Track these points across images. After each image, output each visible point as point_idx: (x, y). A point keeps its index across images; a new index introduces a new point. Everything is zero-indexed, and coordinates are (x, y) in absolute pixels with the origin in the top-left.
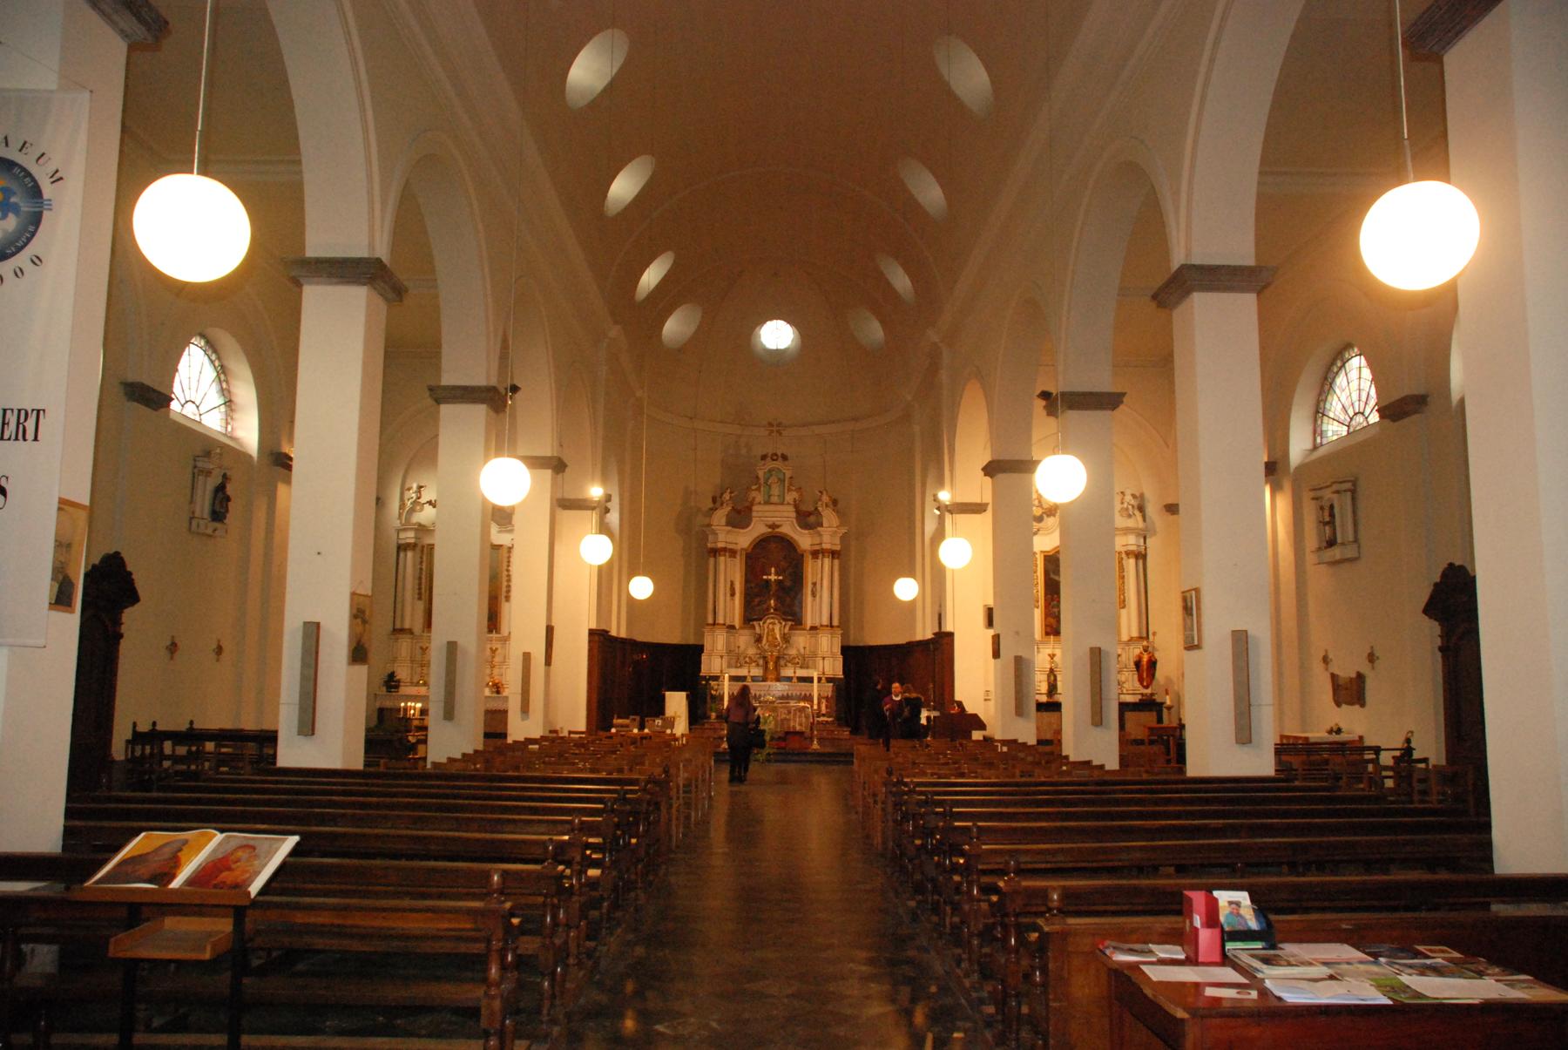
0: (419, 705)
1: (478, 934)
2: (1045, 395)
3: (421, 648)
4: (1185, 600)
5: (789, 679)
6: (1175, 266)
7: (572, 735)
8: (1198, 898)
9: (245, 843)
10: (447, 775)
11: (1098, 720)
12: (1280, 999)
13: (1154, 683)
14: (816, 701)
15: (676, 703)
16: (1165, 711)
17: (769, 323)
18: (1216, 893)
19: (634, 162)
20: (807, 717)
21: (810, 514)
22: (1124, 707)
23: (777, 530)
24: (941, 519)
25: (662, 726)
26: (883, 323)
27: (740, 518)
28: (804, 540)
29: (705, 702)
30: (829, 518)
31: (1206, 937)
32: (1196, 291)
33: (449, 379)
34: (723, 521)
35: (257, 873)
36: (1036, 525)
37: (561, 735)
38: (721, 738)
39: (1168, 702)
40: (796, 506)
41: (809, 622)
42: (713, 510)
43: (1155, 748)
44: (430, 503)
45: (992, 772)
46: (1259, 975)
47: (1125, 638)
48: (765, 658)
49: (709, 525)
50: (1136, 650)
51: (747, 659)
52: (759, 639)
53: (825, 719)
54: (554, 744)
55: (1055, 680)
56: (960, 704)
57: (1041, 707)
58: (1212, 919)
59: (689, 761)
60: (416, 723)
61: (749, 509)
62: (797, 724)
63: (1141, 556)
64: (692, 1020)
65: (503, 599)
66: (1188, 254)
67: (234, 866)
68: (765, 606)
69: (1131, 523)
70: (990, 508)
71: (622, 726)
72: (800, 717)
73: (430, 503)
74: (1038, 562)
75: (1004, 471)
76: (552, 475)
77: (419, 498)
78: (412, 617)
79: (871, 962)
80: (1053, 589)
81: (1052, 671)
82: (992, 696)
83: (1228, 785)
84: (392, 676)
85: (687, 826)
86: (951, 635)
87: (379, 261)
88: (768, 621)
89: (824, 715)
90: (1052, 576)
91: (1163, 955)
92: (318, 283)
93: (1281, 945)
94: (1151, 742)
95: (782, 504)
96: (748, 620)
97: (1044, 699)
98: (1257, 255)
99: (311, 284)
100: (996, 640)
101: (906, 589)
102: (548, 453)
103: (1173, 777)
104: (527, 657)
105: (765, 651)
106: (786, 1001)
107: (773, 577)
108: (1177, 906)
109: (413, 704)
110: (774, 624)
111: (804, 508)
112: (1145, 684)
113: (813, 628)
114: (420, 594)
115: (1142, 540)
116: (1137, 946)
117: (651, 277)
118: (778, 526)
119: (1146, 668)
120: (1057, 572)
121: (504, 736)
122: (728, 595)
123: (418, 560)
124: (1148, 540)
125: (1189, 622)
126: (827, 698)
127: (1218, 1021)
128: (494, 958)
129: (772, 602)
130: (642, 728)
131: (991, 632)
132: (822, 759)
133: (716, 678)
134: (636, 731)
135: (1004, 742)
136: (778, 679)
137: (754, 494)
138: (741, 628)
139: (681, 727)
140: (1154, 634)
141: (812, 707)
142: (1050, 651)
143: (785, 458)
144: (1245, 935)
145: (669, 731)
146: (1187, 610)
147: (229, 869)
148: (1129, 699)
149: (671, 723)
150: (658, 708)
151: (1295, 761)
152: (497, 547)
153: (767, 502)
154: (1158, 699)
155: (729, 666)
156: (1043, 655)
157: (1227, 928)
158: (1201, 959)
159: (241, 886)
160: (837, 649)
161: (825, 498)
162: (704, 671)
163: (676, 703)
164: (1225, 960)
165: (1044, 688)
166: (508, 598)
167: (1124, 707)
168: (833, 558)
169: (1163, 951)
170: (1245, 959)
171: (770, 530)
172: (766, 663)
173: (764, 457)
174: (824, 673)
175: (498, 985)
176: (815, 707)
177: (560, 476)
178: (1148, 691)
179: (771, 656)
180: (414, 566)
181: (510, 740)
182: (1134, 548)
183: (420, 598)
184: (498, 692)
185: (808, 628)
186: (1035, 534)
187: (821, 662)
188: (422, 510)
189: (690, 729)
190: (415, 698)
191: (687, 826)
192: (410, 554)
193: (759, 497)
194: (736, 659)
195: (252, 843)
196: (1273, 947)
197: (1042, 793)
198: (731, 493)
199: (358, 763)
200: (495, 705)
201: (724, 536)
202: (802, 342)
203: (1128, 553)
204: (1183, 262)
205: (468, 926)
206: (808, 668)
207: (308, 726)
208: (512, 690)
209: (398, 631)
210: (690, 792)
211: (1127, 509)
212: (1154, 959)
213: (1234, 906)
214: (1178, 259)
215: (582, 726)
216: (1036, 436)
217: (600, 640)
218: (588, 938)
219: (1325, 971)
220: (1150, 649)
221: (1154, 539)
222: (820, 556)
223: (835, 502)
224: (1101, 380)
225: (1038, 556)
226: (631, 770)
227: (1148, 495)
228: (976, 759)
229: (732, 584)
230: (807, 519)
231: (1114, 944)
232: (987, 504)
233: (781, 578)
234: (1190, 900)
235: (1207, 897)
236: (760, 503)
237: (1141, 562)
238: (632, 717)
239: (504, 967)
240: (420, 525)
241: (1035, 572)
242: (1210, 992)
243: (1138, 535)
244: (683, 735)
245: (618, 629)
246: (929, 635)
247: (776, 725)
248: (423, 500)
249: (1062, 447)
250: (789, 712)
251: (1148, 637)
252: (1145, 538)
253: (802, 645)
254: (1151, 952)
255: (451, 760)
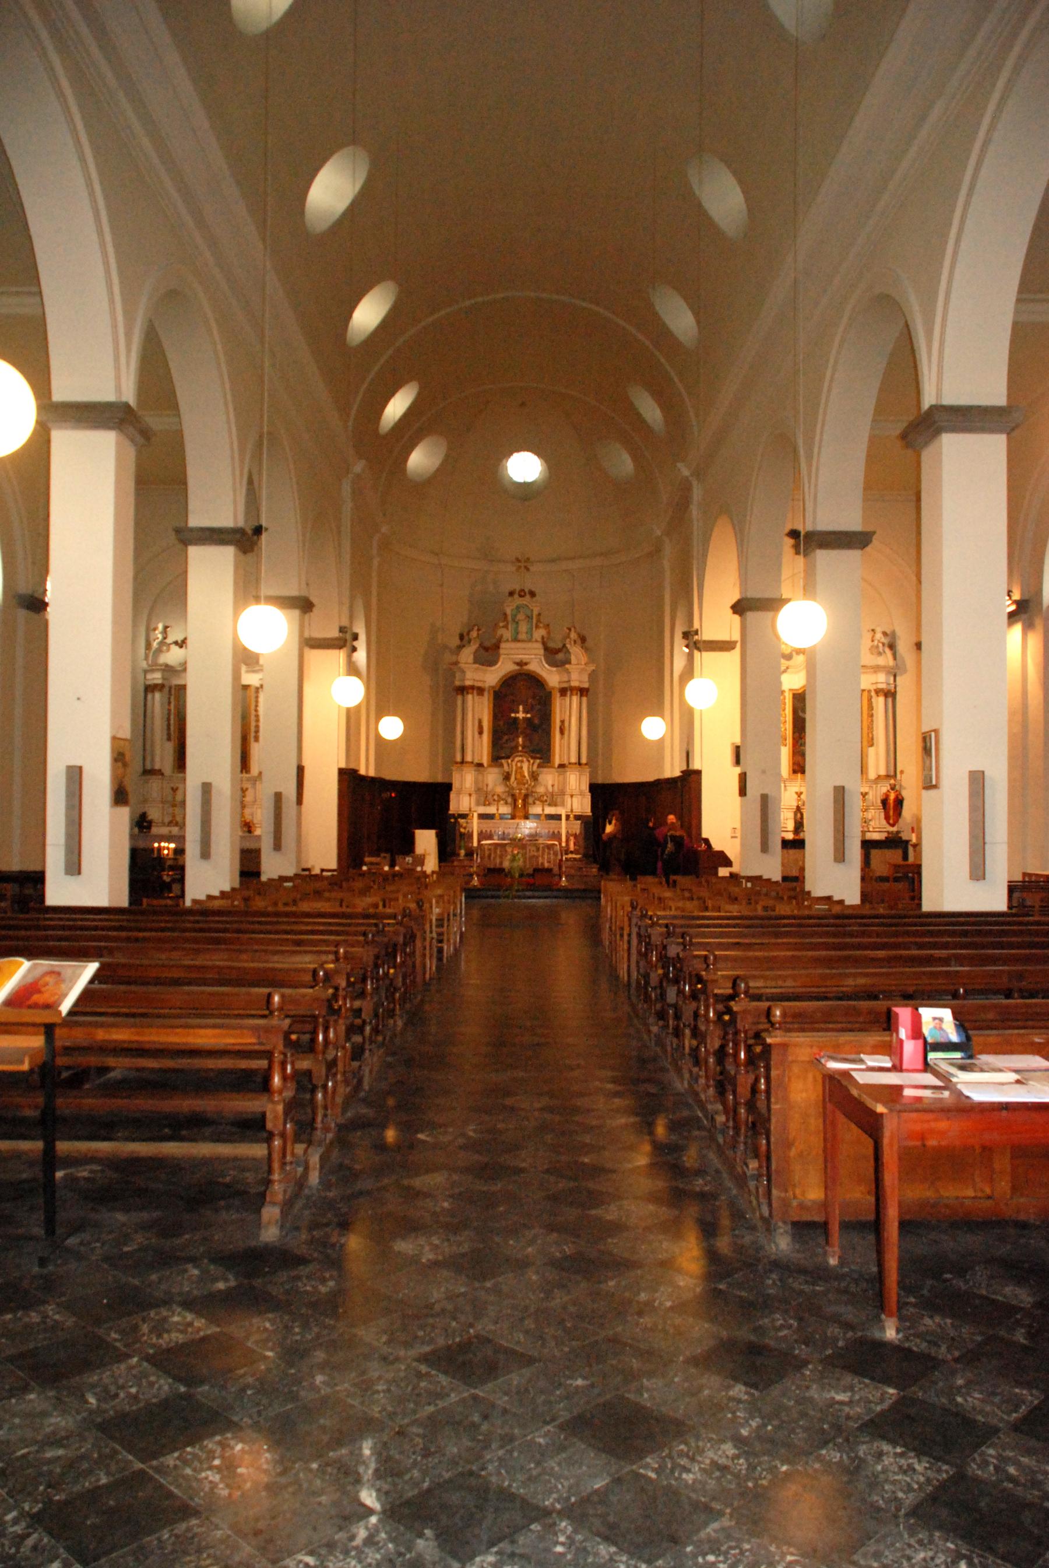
0: (172, 846)
1: (262, 1048)
2: (794, 534)
3: (172, 789)
4: (924, 739)
5: (538, 816)
6: (926, 404)
7: (325, 874)
8: (904, 1014)
9: (50, 969)
10: (203, 911)
11: (840, 856)
12: (968, 1097)
13: (900, 820)
14: (564, 839)
15: (426, 841)
16: (911, 849)
17: (515, 455)
18: (921, 1010)
19: (335, 157)
20: (555, 854)
21: (558, 651)
22: (868, 845)
23: (525, 667)
24: (690, 657)
25: (412, 864)
26: (635, 458)
27: (488, 654)
28: (553, 678)
29: (454, 840)
30: (577, 654)
31: (910, 1048)
32: (946, 432)
33: (196, 520)
34: (471, 659)
35: (65, 995)
36: (784, 663)
37: (313, 873)
38: (471, 875)
39: (914, 840)
40: (544, 643)
41: (557, 762)
42: (460, 647)
43: (900, 886)
44: (176, 643)
45: (736, 906)
46: (954, 1080)
47: (872, 775)
48: (513, 796)
49: (456, 663)
50: (883, 788)
51: (496, 797)
52: (507, 777)
53: (574, 856)
54: (306, 878)
55: (802, 818)
56: (707, 841)
57: (786, 844)
58: (917, 1033)
59: (441, 896)
60: (169, 863)
61: (497, 647)
62: (546, 861)
63: (890, 694)
64: (451, 1130)
65: (252, 740)
66: (939, 394)
67: (43, 989)
68: (513, 744)
69: (881, 661)
70: (738, 645)
71: (372, 864)
72: (549, 854)
73: (176, 643)
74: (787, 701)
75: (751, 609)
76: (236, 556)
77: (165, 638)
78: (163, 756)
79: (614, 1081)
80: (799, 726)
81: (798, 809)
82: (738, 834)
83: (962, 919)
84: (143, 816)
85: (440, 959)
86: (698, 773)
87: (127, 405)
88: (517, 759)
89: (572, 852)
90: (801, 714)
91: (871, 1064)
92: (66, 428)
93: (979, 1056)
94: (896, 880)
95: (530, 641)
96: (496, 758)
97: (790, 836)
98: (1009, 396)
99: (60, 428)
100: (743, 778)
101: (653, 728)
102: (295, 593)
103: (911, 913)
104: (278, 797)
105: (513, 788)
106: (536, 1113)
107: (521, 715)
108: (889, 1023)
109: (166, 845)
110: (522, 761)
111: (551, 645)
112: (891, 821)
113: (562, 766)
114: (169, 735)
115: (892, 679)
116: (853, 1056)
117: (396, 407)
118: (526, 664)
119: (893, 806)
120: (804, 711)
121: (258, 874)
122: (476, 733)
123: (166, 700)
124: (898, 678)
125: (928, 762)
126: (575, 836)
127: (914, 1115)
128: (277, 1068)
129: (520, 740)
130: (392, 865)
131: (738, 770)
132: (568, 894)
133: (464, 816)
134: (386, 868)
135: (749, 879)
136: (526, 817)
137: (501, 631)
138: (490, 766)
139: (431, 865)
140: (902, 772)
141: (560, 844)
142: (797, 789)
143: (532, 594)
144: (947, 1047)
145: (419, 869)
146: (927, 751)
147: (39, 992)
148: (876, 836)
149: (421, 860)
150: (408, 845)
151: (1033, 900)
152: (246, 687)
153: (516, 640)
154: (905, 836)
155: (478, 804)
156: (788, 797)
157: (929, 1040)
158: (905, 1067)
159: (51, 1007)
160: (585, 787)
161: (573, 635)
162: (453, 809)
163: (426, 841)
164: (926, 1067)
165: (790, 825)
166: (257, 739)
167: (868, 845)
168: (581, 695)
169: (872, 1061)
170: (944, 1067)
171: (517, 668)
172: (515, 801)
173: (511, 594)
174: (572, 811)
175: (280, 1092)
176: (564, 844)
177: (307, 616)
178: (895, 829)
179: (520, 793)
180: (162, 705)
181: (264, 878)
182: (883, 686)
183: (169, 739)
184: (250, 832)
185: (556, 765)
186: (785, 671)
187: (569, 800)
188: (168, 650)
189: (440, 867)
190: (169, 839)
191: (440, 959)
192: (157, 695)
193: (507, 634)
194: (484, 796)
195: (57, 969)
196: (971, 1057)
197: (785, 926)
198: (479, 630)
199: (124, 902)
200: (250, 845)
201: (473, 675)
202: (550, 477)
203: (878, 692)
204: (934, 402)
205: (254, 1040)
206: (556, 805)
207: (74, 866)
208: (263, 830)
209: (149, 772)
210: (442, 926)
211: (877, 647)
212: (863, 1067)
213: (937, 1021)
214: (928, 400)
215: (333, 865)
216: (786, 573)
217: (349, 778)
218: (353, 1059)
219: (1014, 1077)
220: (897, 787)
221: (904, 677)
222: (569, 693)
223: (583, 639)
224: (851, 520)
225: (787, 694)
226: (384, 906)
227: (899, 632)
228: (721, 895)
229: (480, 722)
230: (555, 655)
231: (828, 1053)
232: (735, 642)
233: (529, 716)
234: (897, 1014)
235: (912, 1013)
236: (507, 641)
237: (890, 700)
238: (382, 855)
239: (284, 1078)
240: (167, 665)
241: (784, 710)
242: (908, 1092)
243: (888, 673)
244: (433, 872)
245: (367, 768)
246: (677, 773)
247: (525, 862)
248: (169, 640)
249: (809, 590)
250: (538, 849)
251: (895, 776)
252: (895, 676)
253: (550, 783)
254: (862, 1061)
255: (210, 897)
